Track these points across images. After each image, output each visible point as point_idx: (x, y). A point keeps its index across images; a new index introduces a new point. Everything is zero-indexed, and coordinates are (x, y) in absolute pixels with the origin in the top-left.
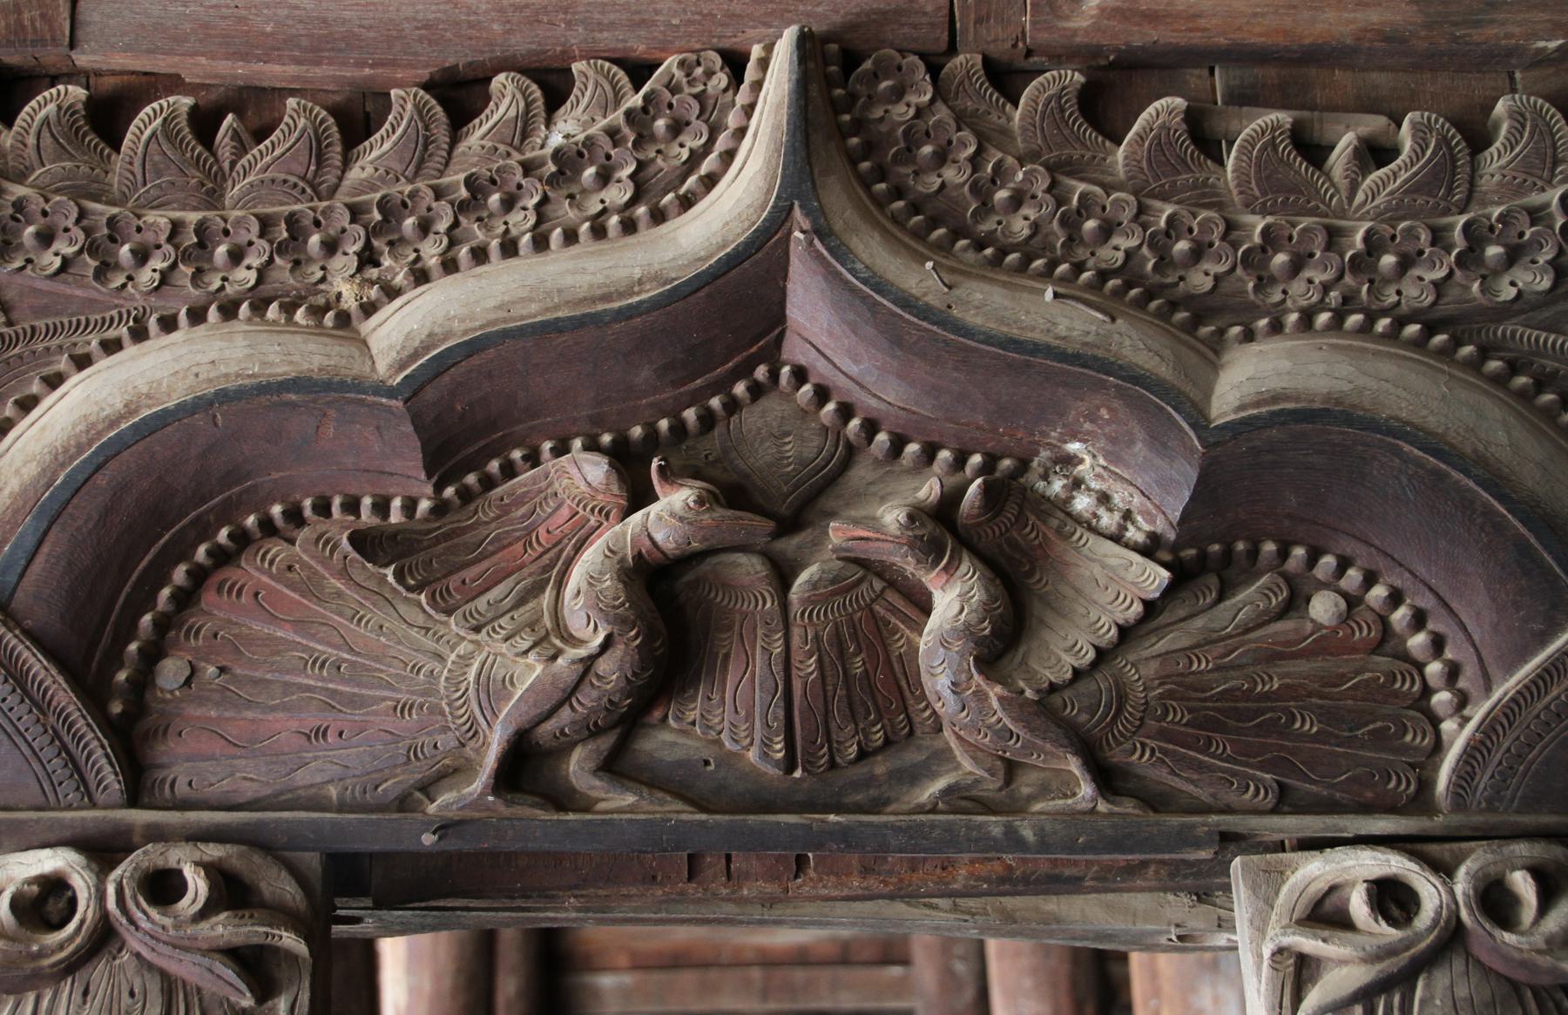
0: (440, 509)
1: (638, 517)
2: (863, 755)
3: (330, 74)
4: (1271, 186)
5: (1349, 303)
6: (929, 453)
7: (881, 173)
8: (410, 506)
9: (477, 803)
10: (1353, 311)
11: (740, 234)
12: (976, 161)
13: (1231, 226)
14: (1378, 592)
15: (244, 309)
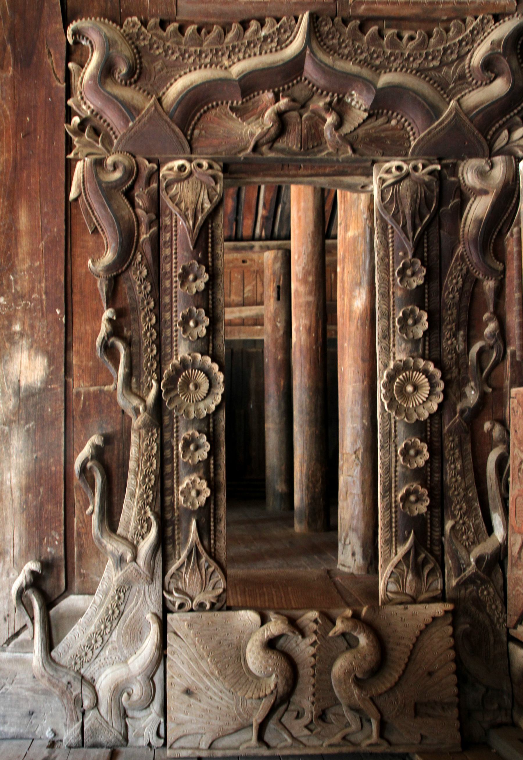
0: (243, 103)
1: (277, 104)
2: (313, 147)
3: (222, 20)
4: (392, 44)
5: (403, 67)
6: (327, 94)
7: (322, 40)
8: (237, 103)
9: (249, 154)
10: (404, 68)
11: (297, 52)
12: (339, 39)
13: (384, 52)
14: (403, 120)
15: (208, 66)
